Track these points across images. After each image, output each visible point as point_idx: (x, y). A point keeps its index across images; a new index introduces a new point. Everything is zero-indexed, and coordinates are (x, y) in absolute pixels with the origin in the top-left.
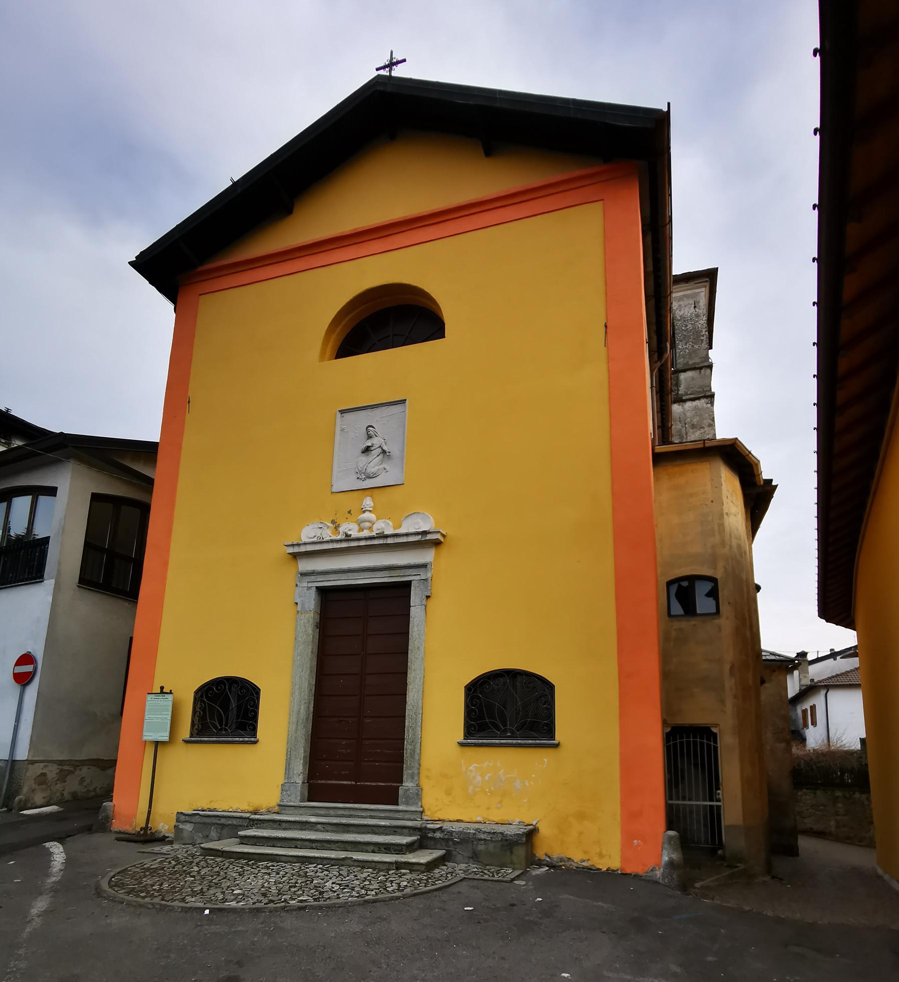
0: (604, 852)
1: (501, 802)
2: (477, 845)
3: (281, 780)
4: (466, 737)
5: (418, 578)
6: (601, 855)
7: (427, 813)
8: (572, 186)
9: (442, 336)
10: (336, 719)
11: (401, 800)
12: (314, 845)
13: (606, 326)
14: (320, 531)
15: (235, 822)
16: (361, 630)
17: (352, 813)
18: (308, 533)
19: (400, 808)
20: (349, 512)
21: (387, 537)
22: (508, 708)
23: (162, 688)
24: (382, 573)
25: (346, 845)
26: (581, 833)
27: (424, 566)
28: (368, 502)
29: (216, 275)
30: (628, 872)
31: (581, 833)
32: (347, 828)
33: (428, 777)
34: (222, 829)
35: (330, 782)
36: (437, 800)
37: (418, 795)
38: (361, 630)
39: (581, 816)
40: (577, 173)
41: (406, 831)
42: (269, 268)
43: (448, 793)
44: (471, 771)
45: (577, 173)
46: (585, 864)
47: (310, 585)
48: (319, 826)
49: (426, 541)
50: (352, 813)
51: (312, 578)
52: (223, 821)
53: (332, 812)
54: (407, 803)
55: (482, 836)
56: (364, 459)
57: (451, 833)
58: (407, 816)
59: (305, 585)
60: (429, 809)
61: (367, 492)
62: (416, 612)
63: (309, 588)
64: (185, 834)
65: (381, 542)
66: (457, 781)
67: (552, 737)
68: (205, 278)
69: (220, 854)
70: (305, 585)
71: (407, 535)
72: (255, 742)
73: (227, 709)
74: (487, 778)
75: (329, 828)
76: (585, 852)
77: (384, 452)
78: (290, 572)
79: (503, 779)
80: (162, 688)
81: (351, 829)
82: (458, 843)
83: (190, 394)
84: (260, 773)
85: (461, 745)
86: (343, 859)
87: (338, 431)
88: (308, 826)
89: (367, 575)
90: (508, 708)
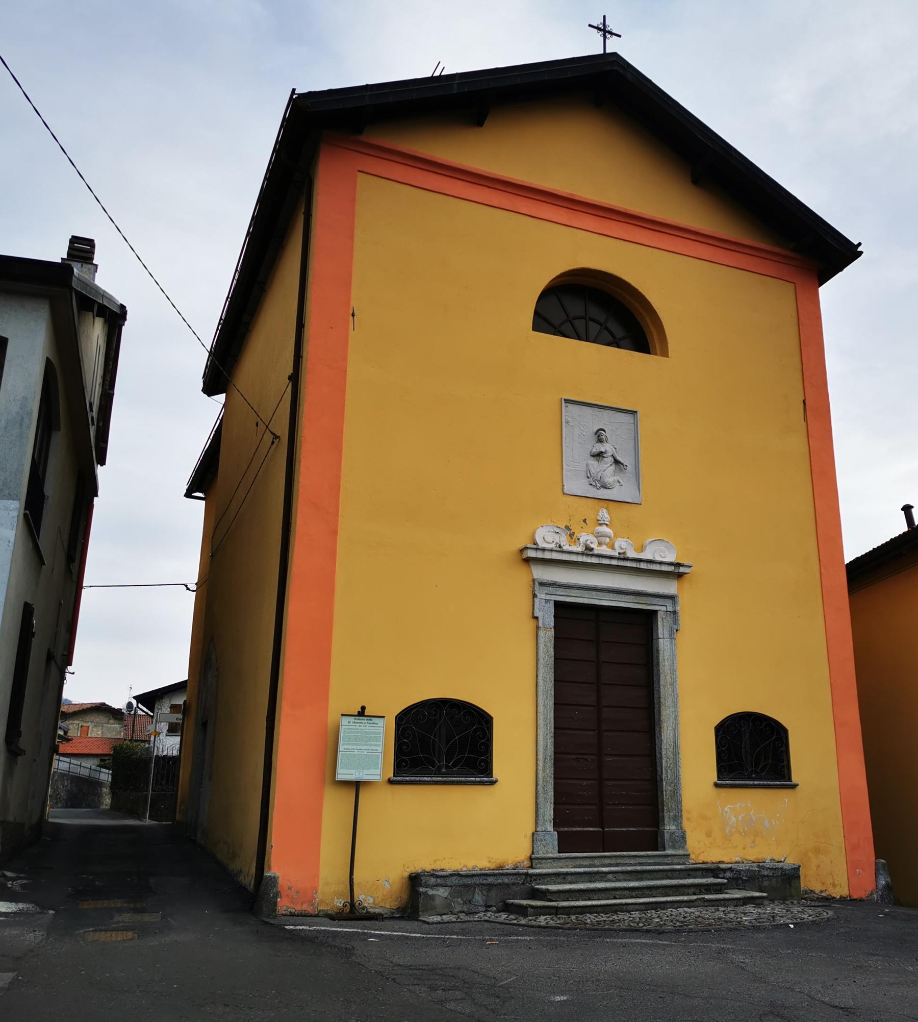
0: (836, 882)
1: (753, 842)
2: (762, 882)
3: (530, 829)
4: (719, 778)
5: (664, 608)
6: (834, 885)
7: (692, 856)
8: (773, 258)
9: (533, 330)
10: (573, 757)
11: (667, 844)
12: (634, 894)
13: (804, 402)
14: (557, 536)
15: (506, 880)
16: (606, 655)
17: (619, 861)
18: (547, 537)
19: (669, 852)
20: (585, 521)
21: (627, 559)
22: (753, 750)
23: (363, 708)
24: (628, 597)
25: (668, 890)
26: (818, 866)
27: (672, 598)
28: (604, 514)
29: (419, 165)
30: (855, 897)
31: (818, 866)
32: (640, 876)
33: (688, 819)
34: (489, 890)
35: (574, 829)
36: (699, 842)
37: (681, 840)
38: (606, 655)
39: (817, 851)
40: (763, 246)
41: (699, 873)
42: (638, 230)
43: (708, 835)
44: (727, 812)
45: (776, 249)
46: (824, 894)
47: (548, 597)
48: (610, 876)
49: (676, 572)
50: (619, 861)
51: (551, 589)
52: (490, 880)
53: (597, 862)
54: (674, 847)
55: (766, 873)
56: (593, 463)
57: (739, 871)
58: (675, 861)
59: (543, 596)
60: (693, 853)
61: (602, 503)
62: (664, 644)
63: (547, 601)
64: (438, 902)
65: (621, 563)
66: (716, 823)
67: (790, 779)
68: (365, 151)
69: (554, 911)
70: (543, 596)
71: (661, 563)
72: (493, 783)
73: (443, 742)
74: (740, 818)
75: (621, 876)
76: (823, 884)
77: (617, 462)
78: (519, 580)
79: (754, 818)
80: (363, 708)
81: (646, 875)
82: (746, 881)
83: (353, 303)
84: (499, 821)
85: (716, 785)
86: (696, 900)
87: (564, 424)
88: (597, 877)
89: (611, 596)
90: (753, 750)
